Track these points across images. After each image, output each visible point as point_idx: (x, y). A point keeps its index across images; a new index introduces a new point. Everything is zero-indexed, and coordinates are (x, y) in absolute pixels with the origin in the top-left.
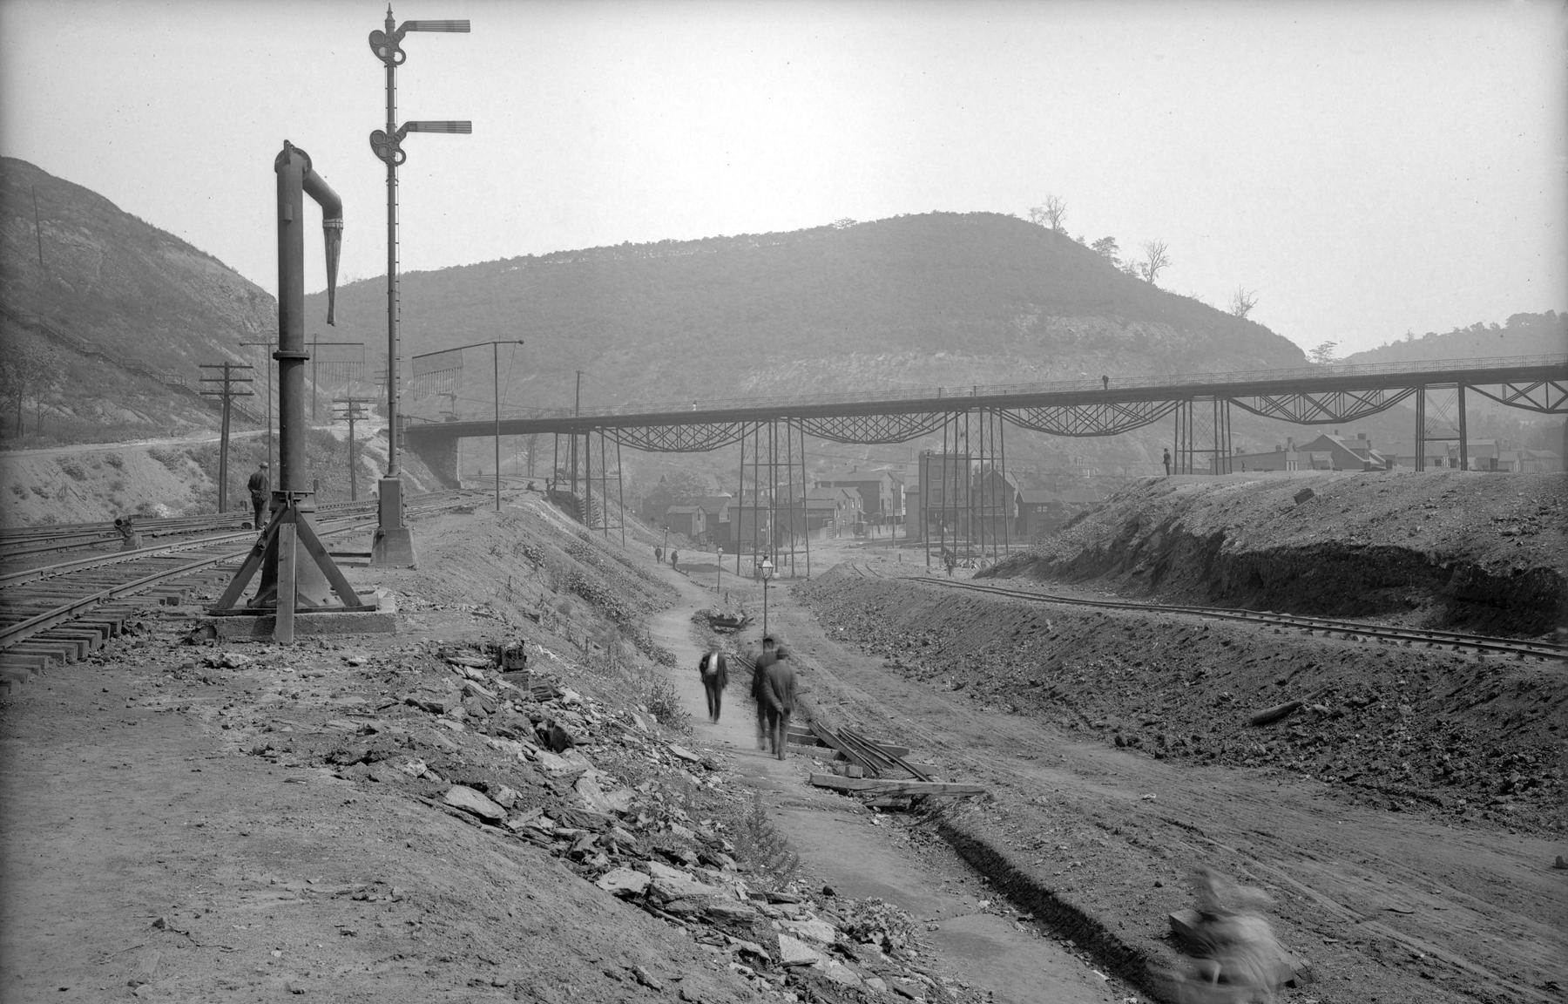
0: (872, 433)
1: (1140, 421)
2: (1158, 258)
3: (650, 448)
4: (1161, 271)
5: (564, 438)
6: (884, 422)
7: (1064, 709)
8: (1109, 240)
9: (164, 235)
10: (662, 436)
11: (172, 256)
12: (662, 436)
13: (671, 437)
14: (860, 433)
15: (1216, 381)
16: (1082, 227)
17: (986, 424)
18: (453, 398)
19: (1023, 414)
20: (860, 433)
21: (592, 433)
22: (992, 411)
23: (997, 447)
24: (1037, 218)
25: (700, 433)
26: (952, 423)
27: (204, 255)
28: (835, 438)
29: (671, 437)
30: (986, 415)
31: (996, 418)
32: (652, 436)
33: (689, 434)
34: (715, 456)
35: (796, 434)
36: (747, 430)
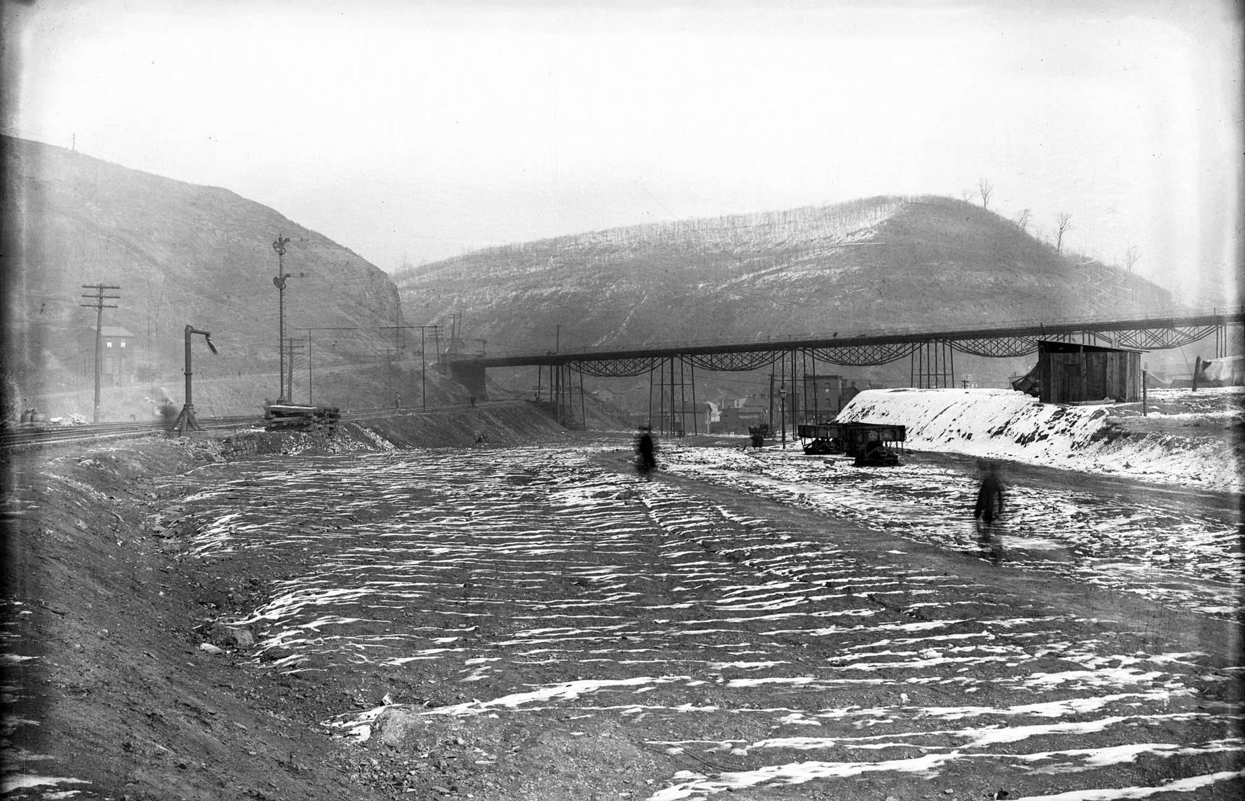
0: (862, 358)
1: (899, 356)
2: (1131, 259)
3: (713, 368)
4: (1135, 265)
5: (547, 368)
6: (870, 351)
7: (1151, 609)
8: (1026, 211)
9: (315, 235)
10: (721, 361)
11: (320, 250)
12: (721, 361)
13: (727, 361)
14: (853, 358)
15: (782, 341)
16: (1005, 207)
17: (932, 353)
18: (485, 342)
19: (963, 343)
20: (853, 358)
21: (675, 359)
22: (944, 342)
23: (948, 365)
24: (968, 197)
25: (746, 359)
26: (917, 352)
27: (340, 247)
28: (836, 362)
29: (727, 361)
30: (939, 344)
31: (947, 348)
32: (714, 360)
33: (738, 360)
34: (755, 374)
35: (687, 367)
36: (656, 364)
